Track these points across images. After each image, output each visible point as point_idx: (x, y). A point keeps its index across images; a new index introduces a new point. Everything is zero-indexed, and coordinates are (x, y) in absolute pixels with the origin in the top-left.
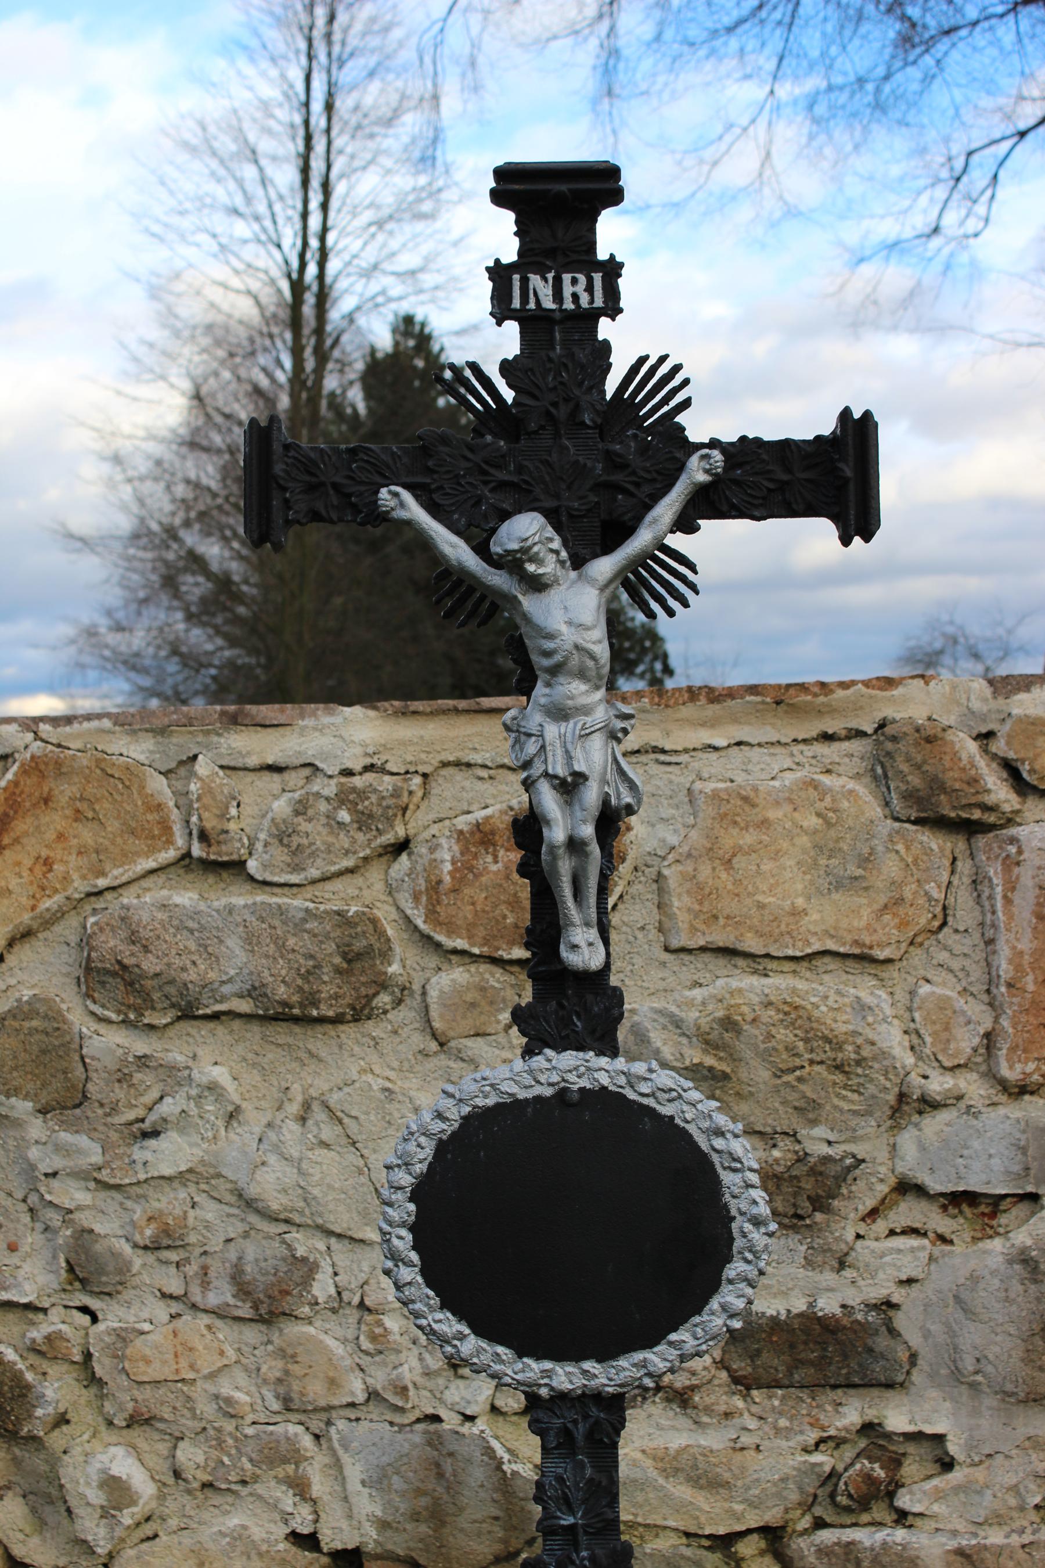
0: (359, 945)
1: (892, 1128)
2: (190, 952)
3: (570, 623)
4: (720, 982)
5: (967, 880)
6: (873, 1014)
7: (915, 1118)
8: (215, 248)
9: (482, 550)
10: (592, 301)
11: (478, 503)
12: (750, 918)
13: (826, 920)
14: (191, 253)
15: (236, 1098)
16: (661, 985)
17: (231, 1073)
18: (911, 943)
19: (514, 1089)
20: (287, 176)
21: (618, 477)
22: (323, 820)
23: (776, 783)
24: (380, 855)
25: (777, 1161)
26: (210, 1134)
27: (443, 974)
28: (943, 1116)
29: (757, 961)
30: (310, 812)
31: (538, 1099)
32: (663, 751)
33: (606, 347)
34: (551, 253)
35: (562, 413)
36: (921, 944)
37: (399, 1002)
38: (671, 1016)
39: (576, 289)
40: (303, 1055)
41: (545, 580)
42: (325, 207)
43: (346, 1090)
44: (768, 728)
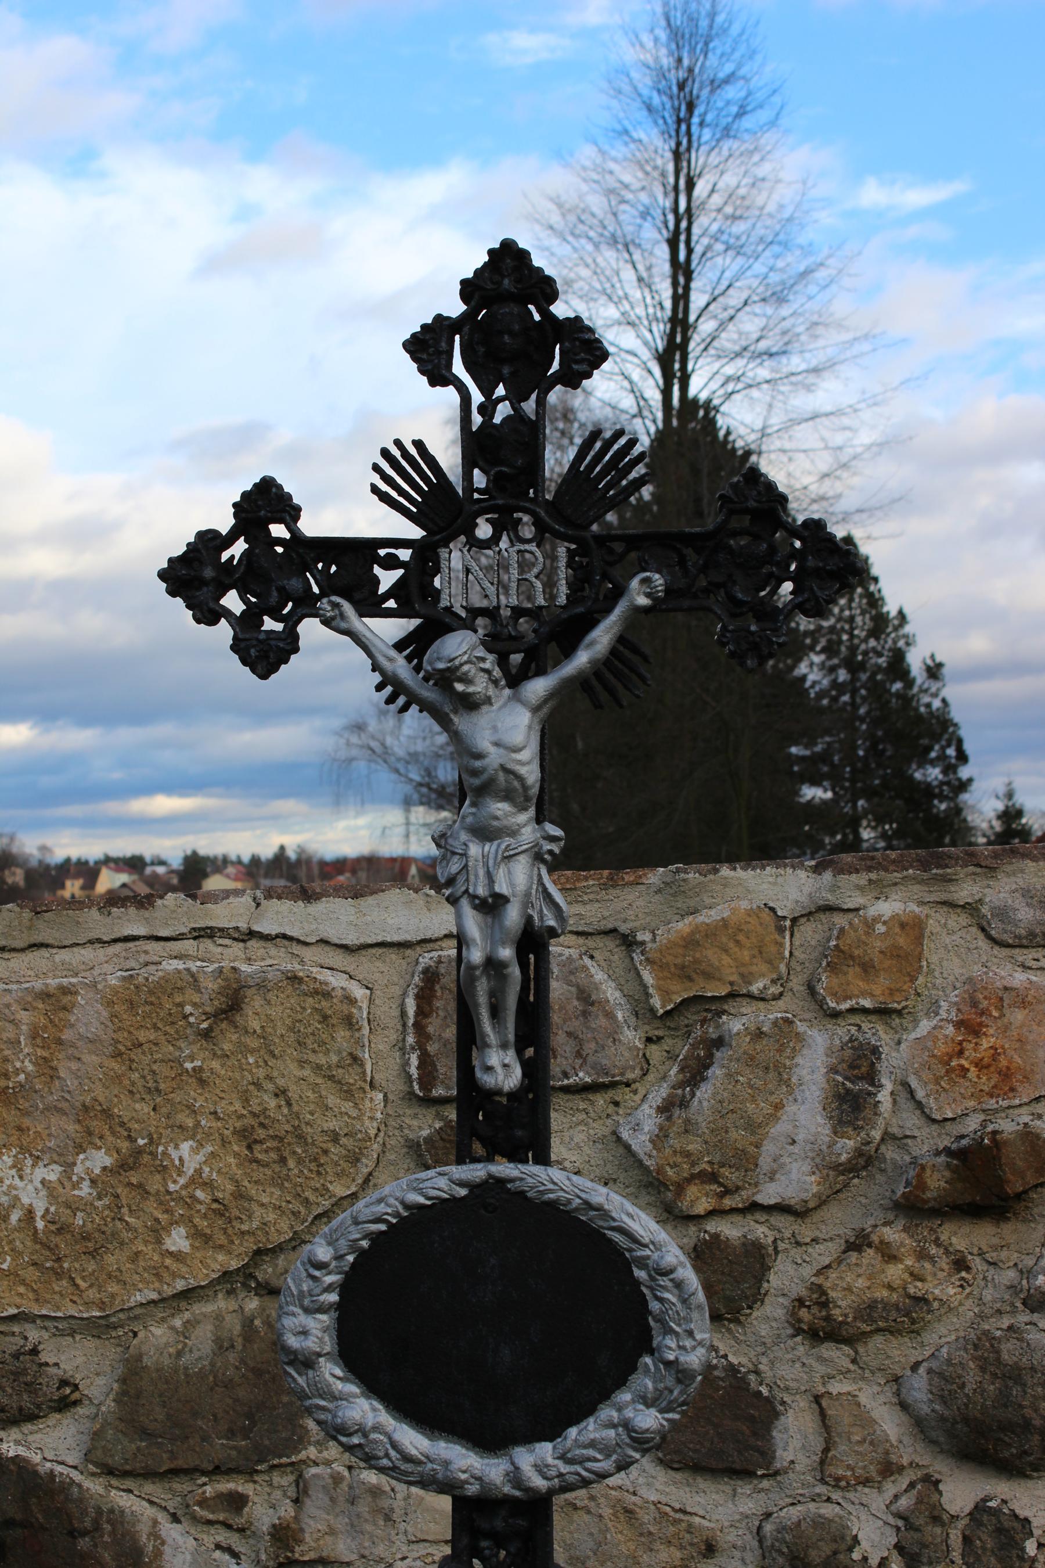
3: (497, 744)
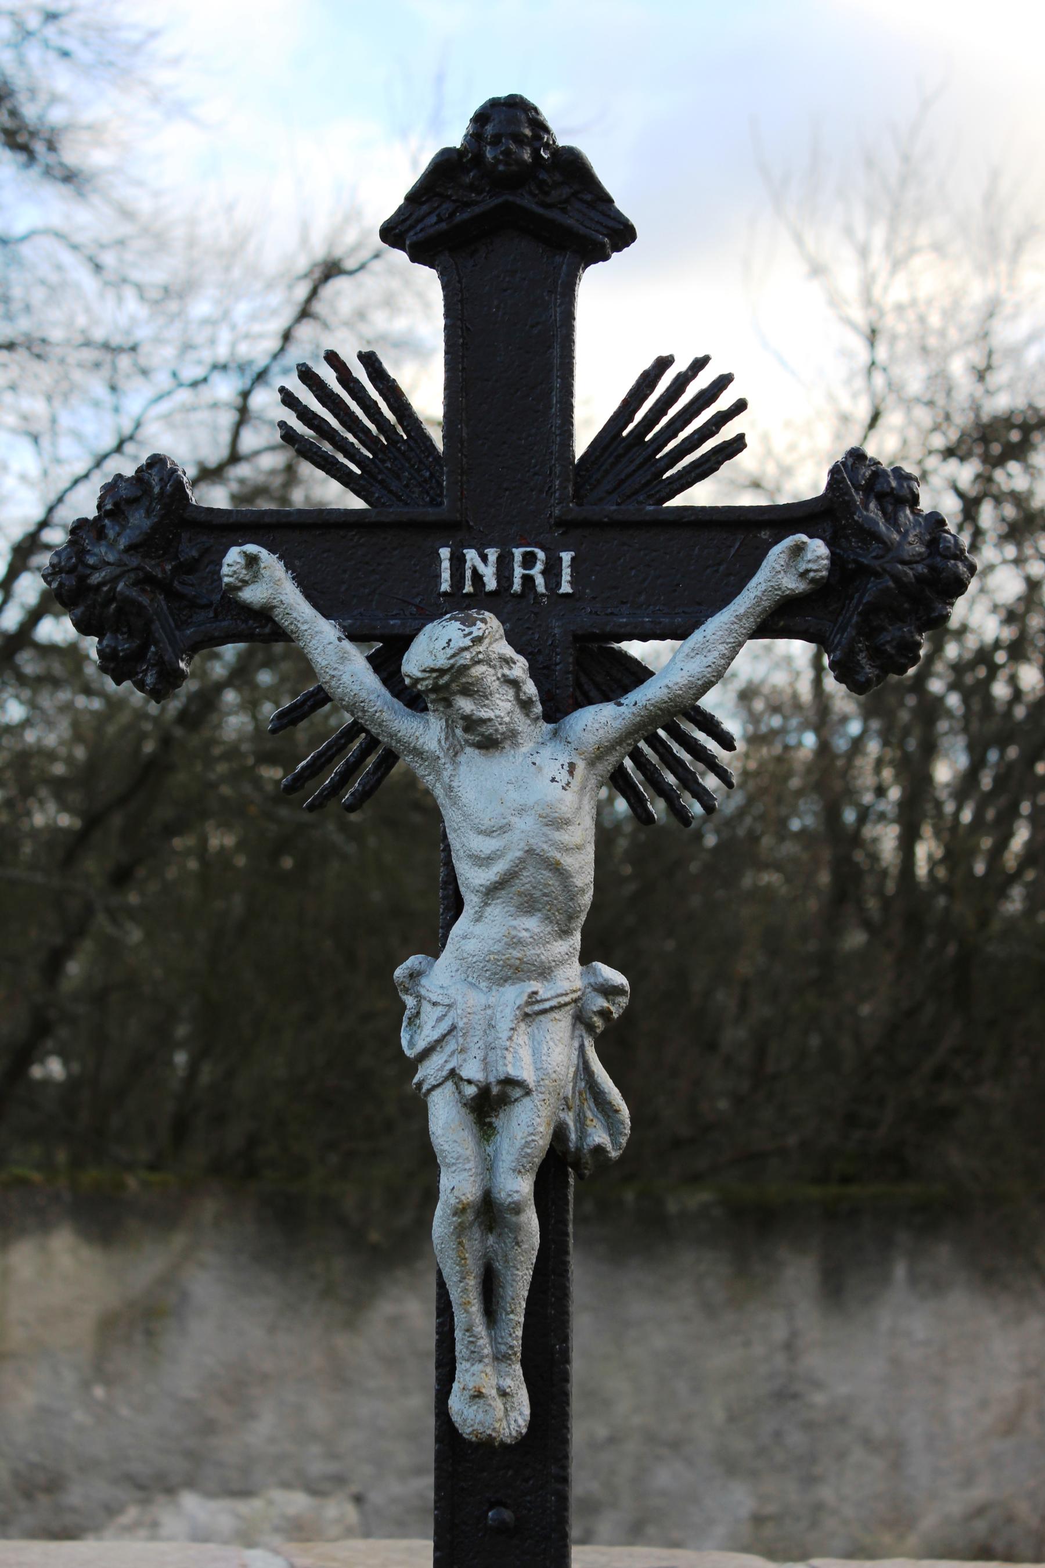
9: (387, 664)
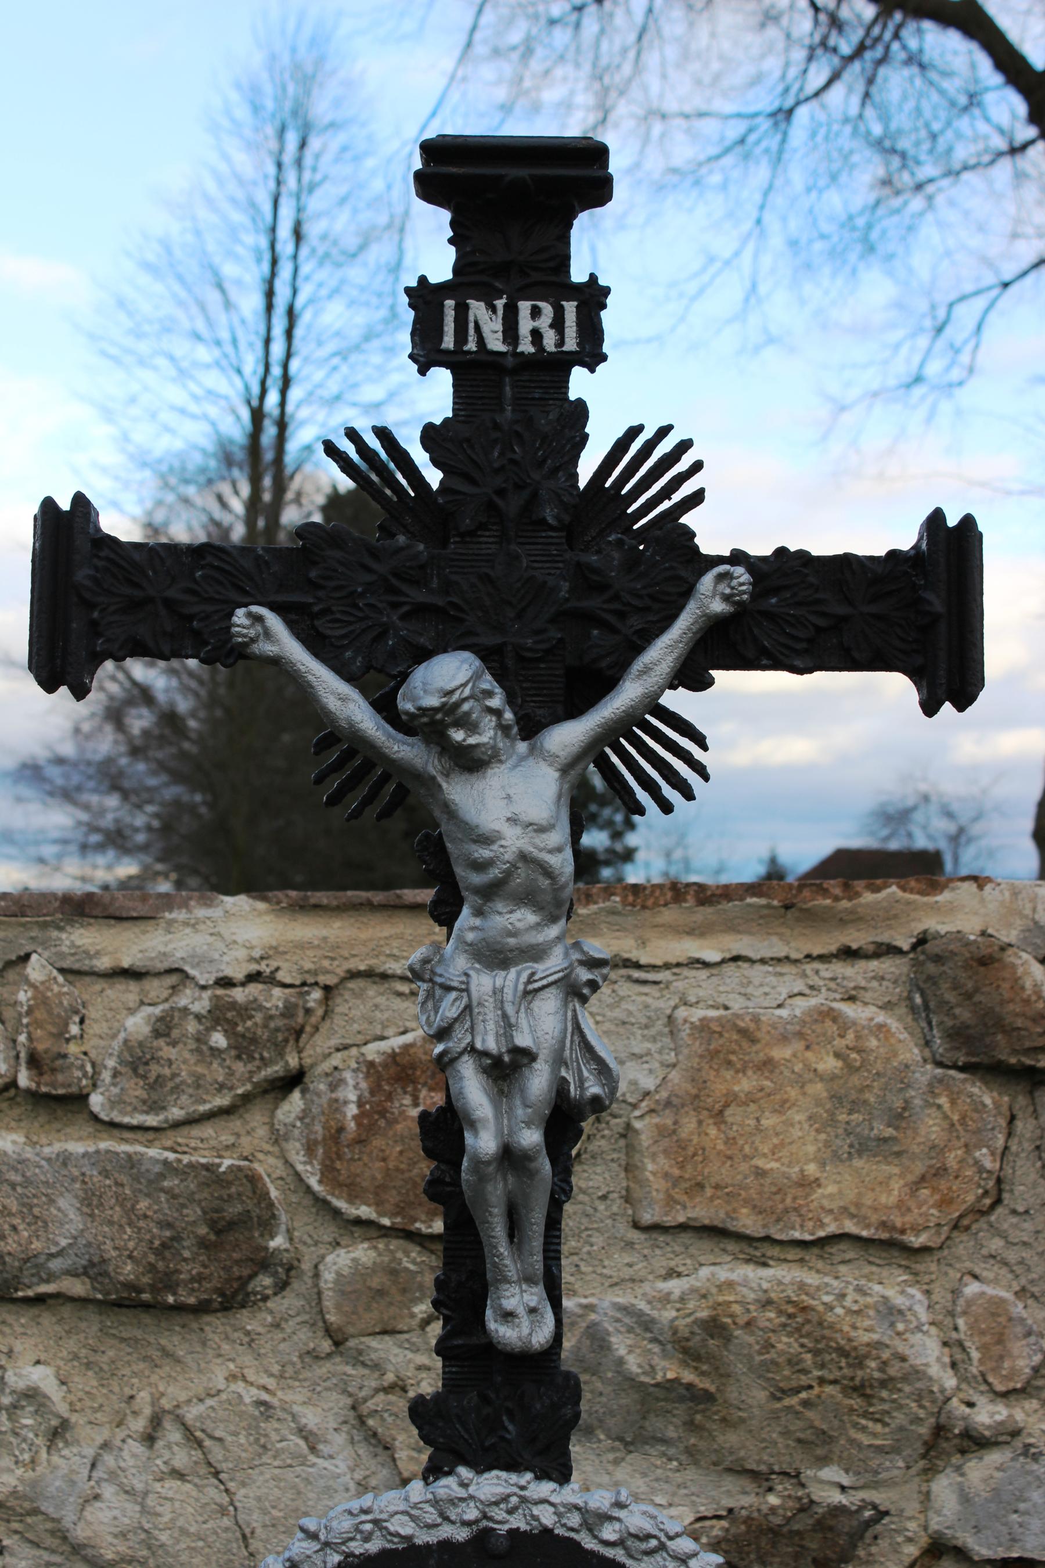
0: (234, 1210)
1: (925, 1471)
2: (11, 1214)
3: (513, 820)
4: (705, 1272)
5: (1028, 1146)
6: (905, 1318)
7: (956, 1459)
8: (173, 373)
9: (385, 706)
10: (561, 342)
11: (382, 636)
12: (746, 1188)
13: (847, 1191)
14: (148, 376)
15: (63, 1409)
16: (627, 1273)
17: (57, 1376)
18: (955, 1227)
19: (406, 1528)
20: (251, 303)
21: (594, 603)
22: (192, 1045)
23: (784, 1013)
24: (265, 1092)
25: (773, 1509)
26: (27, 1457)
27: (342, 1252)
28: (995, 1457)
29: (757, 1247)
30: (175, 1033)
31: (446, 1545)
32: (638, 966)
33: (580, 410)
34: (502, 270)
35: (511, 506)
36: (967, 1228)
37: (282, 1286)
38: (640, 1314)
39: (535, 320)
40: (156, 1354)
41: (478, 754)
42: (289, 334)
43: (210, 1402)
44: (775, 939)
